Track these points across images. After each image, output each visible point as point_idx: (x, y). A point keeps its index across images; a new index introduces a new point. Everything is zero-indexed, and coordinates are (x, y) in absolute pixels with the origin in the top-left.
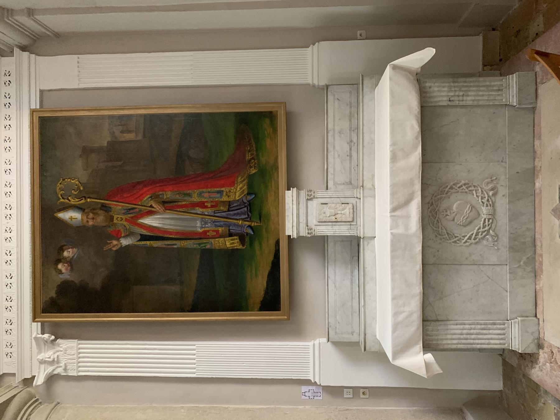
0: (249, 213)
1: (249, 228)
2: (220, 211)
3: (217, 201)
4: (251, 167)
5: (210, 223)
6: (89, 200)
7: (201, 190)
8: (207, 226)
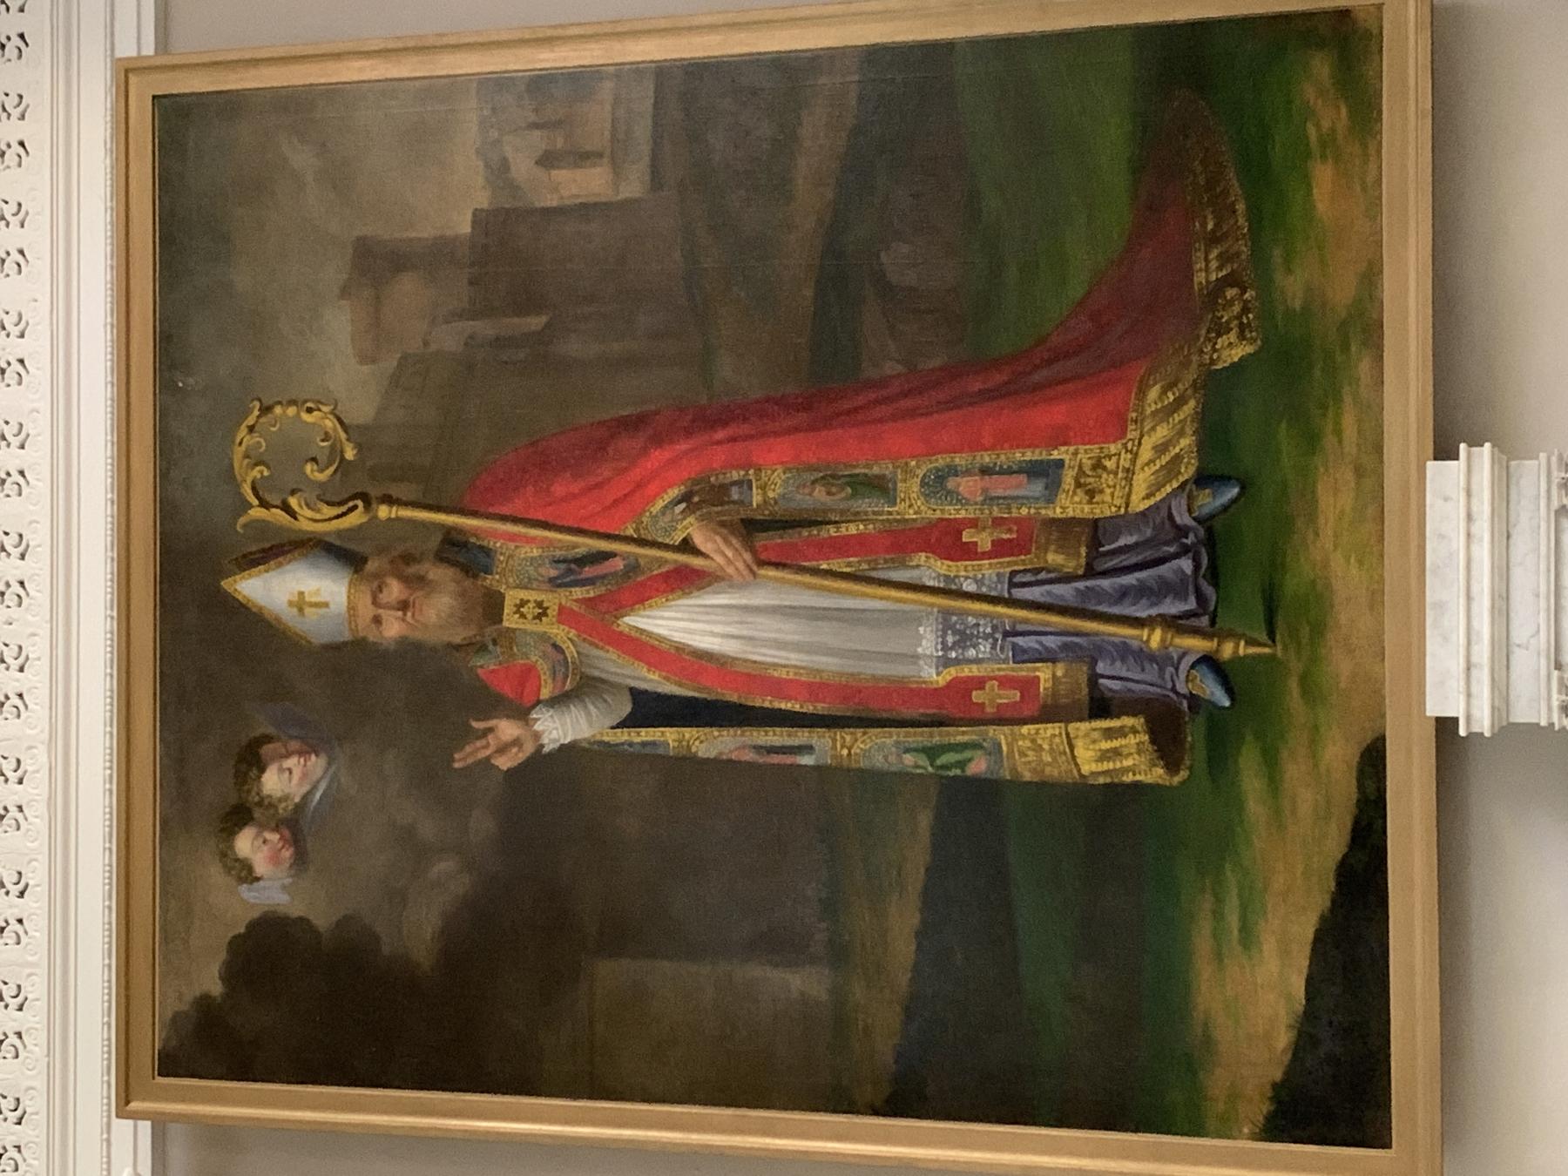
0: (1209, 591)
1: (1204, 668)
2: (1043, 576)
3: (1029, 518)
4: (1221, 330)
5: (986, 637)
6: (383, 512)
7: (941, 461)
8: (972, 653)
